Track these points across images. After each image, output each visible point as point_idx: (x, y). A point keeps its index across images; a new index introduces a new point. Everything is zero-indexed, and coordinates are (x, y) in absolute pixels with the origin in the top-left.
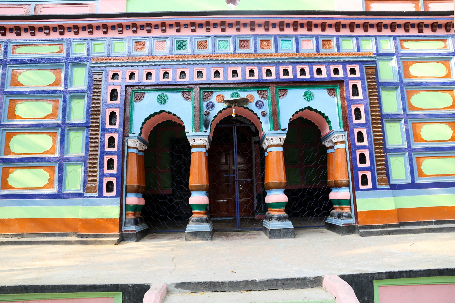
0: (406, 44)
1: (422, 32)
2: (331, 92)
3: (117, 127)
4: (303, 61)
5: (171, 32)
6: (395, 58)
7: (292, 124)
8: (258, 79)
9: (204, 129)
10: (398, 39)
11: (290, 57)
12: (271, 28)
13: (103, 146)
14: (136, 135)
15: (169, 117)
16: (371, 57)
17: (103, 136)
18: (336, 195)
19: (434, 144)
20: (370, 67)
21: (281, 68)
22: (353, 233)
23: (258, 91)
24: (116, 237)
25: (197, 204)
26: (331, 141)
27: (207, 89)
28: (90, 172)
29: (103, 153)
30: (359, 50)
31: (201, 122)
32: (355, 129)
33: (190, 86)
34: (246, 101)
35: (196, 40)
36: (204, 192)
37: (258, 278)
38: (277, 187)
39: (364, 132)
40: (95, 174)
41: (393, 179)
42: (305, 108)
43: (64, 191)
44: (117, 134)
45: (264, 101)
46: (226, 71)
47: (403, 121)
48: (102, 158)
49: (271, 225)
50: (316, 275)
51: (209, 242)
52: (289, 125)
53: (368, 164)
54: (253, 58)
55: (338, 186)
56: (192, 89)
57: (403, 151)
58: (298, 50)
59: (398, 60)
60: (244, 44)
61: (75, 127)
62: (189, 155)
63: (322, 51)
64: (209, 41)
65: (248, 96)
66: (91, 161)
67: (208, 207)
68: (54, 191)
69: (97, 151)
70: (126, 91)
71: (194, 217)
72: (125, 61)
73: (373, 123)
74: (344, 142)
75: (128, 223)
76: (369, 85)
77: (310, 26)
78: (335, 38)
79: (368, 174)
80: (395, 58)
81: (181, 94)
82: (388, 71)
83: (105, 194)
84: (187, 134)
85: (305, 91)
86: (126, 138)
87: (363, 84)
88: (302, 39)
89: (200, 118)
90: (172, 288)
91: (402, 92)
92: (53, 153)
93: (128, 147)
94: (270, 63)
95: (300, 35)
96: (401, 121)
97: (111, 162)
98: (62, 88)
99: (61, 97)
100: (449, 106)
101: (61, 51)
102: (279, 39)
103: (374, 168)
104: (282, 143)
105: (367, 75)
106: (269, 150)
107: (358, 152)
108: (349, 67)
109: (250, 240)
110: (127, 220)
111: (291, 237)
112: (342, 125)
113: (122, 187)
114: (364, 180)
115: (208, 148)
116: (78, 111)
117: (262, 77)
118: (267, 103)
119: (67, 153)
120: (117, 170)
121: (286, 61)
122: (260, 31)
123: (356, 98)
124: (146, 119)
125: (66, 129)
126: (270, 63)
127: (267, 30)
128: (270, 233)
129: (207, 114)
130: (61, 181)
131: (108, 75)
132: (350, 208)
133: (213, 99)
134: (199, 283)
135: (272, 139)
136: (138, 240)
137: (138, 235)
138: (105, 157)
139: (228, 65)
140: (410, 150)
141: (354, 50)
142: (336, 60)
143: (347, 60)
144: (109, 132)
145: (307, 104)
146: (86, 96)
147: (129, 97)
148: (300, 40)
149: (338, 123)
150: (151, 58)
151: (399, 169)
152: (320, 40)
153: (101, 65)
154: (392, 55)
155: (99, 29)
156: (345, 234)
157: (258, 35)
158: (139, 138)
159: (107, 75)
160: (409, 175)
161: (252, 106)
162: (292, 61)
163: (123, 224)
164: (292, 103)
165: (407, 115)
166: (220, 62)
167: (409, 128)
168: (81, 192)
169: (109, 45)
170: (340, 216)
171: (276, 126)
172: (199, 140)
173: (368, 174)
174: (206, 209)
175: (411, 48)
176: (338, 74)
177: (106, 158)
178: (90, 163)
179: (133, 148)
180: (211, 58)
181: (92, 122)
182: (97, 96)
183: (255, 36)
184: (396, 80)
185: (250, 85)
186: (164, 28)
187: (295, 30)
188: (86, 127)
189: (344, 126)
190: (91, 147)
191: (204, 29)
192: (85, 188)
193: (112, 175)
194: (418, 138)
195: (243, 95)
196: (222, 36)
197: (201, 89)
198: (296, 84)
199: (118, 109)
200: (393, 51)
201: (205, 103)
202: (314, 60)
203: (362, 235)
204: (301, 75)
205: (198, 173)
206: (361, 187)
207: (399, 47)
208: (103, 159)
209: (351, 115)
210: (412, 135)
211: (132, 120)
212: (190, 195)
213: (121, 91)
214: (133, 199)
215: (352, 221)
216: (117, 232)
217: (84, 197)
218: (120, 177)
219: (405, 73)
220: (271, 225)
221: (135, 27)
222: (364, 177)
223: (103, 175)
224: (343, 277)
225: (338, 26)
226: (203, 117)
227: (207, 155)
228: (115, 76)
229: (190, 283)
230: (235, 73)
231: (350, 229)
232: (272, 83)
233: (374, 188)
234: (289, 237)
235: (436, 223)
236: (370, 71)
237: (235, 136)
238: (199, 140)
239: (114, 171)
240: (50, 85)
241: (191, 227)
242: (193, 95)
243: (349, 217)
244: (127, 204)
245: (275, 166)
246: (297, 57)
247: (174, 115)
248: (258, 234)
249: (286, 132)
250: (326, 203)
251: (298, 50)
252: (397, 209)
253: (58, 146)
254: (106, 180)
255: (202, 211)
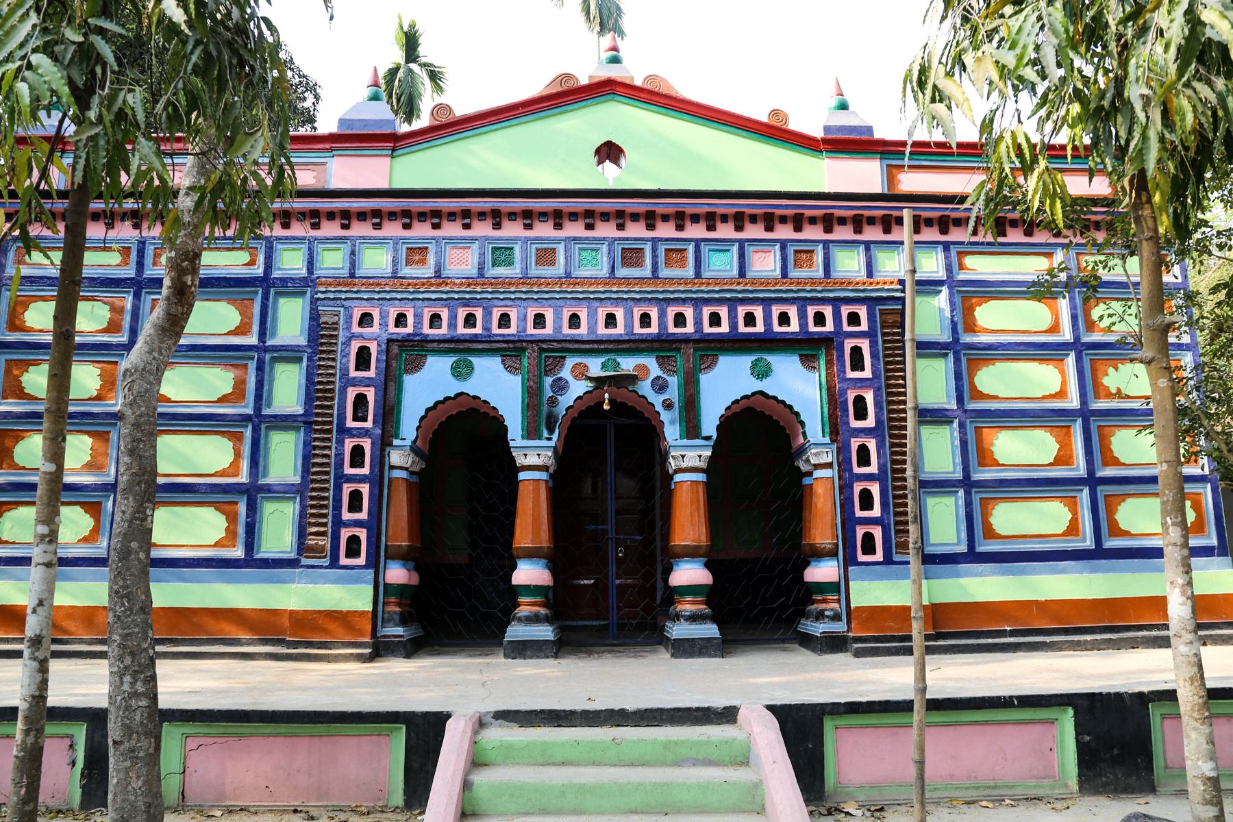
0: (969, 261)
1: (1005, 235)
2: (808, 361)
3: (368, 424)
4: (751, 296)
5: (482, 229)
6: (945, 290)
7: (728, 423)
8: (659, 334)
9: (546, 434)
10: (953, 251)
11: (726, 287)
12: (688, 224)
13: (340, 465)
14: (408, 443)
15: (474, 404)
16: (893, 290)
17: (341, 442)
18: (823, 571)
19: (1018, 471)
20: (889, 314)
21: (706, 311)
22: (841, 651)
23: (657, 357)
24: (365, 647)
25: (529, 586)
26: (808, 461)
27: (553, 352)
28: (312, 515)
29: (341, 479)
30: (870, 274)
31: (538, 416)
32: (853, 440)
33: (519, 345)
34: (632, 379)
35: (534, 246)
36: (544, 561)
37: (631, 705)
38: (691, 553)
39: (872, 445)
40: (324, 520)
41: (932, 541)
42: (754, 394)
43: (258, 552)
44: (369, 441)
45: (668, 378)
46: (592, 316)
47: (956, 424)
48: (338, 488)
49: (678, 630)
50: (728, 704)
51: (551, 661)
52: (718, 428)
53: (876, 512)
54: (648, 289)
55: (820, 554)
56: (523, 350)
57: (954, 486)
58: (742, 273)
59: (951, 294)
60: (632, 256)
61: (284, 422)
62: (514, 484)
63: (794, 273)
64: (561, 249)
65: (637, 367)
66: (314, 494)
67: (550, 596)
68: (238, 553)
69: (327, 473)
70: (388, 350)
71: (523, 611)
72: (388, 289)
73: (891, 428)
74: (829, 465)
75: (389, 620)
76: (886, 349)
77: (769, 222)
78: (820, 246)
79: (877, 532)
80: (945, 290)
81: (499, 359)
82: (930, 317)
83: (344, 561)
84: (512, 444)
85: (753, 358)
86: (388, 449)
87: (873, 345)
88: (752, 248)
89: (539, 411)
90: (489, 719)
91: (957, 361)
92: (236, 475)
93: (392, 467)
94: (684, 301)
95: (748, 240)
96: (952, 422)
97: (356, 497)
98: (252, 340)
99: (252, 358)
100: (1053, 392)
101: (252, 263)
102: (705, 249)
103: (889, 519)
104: (703, 465)
105: (883, 327)
106: (678, 478)
107: (858, 487)
108: (845, 310)
109: (633, 660)
110: (386, 616)
111: (716, 656)
112: (827, 430)
113: (378, 547)
114: (869, 547)
115: (551, 471)
116: (288, 389)
117: (666, 328)
118: (673, 381)
119: (265, 476)
120: (369, 514)
121: (717, 296)
122: (666, 230)
123: (857, 375)
124: (428, 410)
125: (263, 427)
126: (684, 301)
127: (680, 228)
128: (673, 647)
129: (553, 402)
130: (252, 530)
131: (351, 317)
132: (839, 601)
133: (566, 373)
134: (532, 711)
135: (683, 457)
136: (409, 655)
137: (408, 647)
138: (345, 486)
139: (597, 304)
140: (967, 483)
141: (859, 271)
142: (820, 295)
143: (842, 294)
144: (353, 436)
145: (754, 385)
146: (305, 359)
147: (394, 364)
148: (749, 249)
149: (820, 426)
150: (440, 285)
151: (943, 521)
152: (791, 250)
153: (339, 296)
154: (940, 283)
155: (333, 219)
156: (825, 652)
157: (661, 239)
158: (414, 449)
159: (349, 318)
160: (964, 535)
161: (645, 388)
162: (728, 296)
163: (379, 623)
164: (726, 384)
165: (965, 411)
166: (581, 296)
167: (969, 436)
168: (293, 556)
169: (353, 253)
170: (820, 616)
171: (692, 429)
172: (534, 455)
173: (877, 532)
174: (546, 597)
175: (980, 269)
176: (824, 325)
177: (347, 488)
178: (312, 498)
179: (401, 468)
180: (564, 288)
181: (318, 415)
182: (329, 359)
183: (655, 241)
184: (946, 337)
185: (642, 346)
186: (467, 221)
187: (739, 228)
188: (305, 423)
189: (831, 434)
190: (315, 464)
191: (551, 223)
192: (302, 548)
193: (358, 524)
194: (985, 458)
195: (628, 364)
196: (587, 239)
197: (542, 350)
198: (736, 344)
199: (372, 389)
200: (941, 274)
201: (548, 380)
202: (773, 295)
203: (858, 654)
204: (746, 325)
205: (531, 521)
206: (862, 558)
207: (955, 268)
208: (341, 490)
209: (847, 410)
210: (973, 451)
211: (399, 412)
212: (514, 567)
213: (379, 352)
214: (397, 574)
215: (840, 627)
216: (367, 640)
217: (302, 566)
218: (373, 526)
219: (965, 323)
220: (678, 630)
221: (408, 218)
222: (868, 538)
223: (339, 523)
224: (771, 708)
225: (828, 223)
226: (545, 409)
227: (550, 484)
228: (366, 319)
229: (517, 712)
230: (611, 320)
231: (835, 644)
232: (686, 340)
233: (888, 560)
234: (710, 656)
235: (1013, 633)
236: (890, 319)
237: (610, 441)
238: (534, 455)
239: (363, 516)
240: (229, 333)
241: (516, 632)
242: (525, 362)
243: (836, 617)
244: (388, 581)
245: (688, 511)
246: (740, 288)
247: (486, 402)
248: (654, 651)
249: (711, 443)
250: (799, 591)
251: (742, 273)
252: (933, 605)
253: (245, 465)
254: (345, 534)
255: (538, 599)
